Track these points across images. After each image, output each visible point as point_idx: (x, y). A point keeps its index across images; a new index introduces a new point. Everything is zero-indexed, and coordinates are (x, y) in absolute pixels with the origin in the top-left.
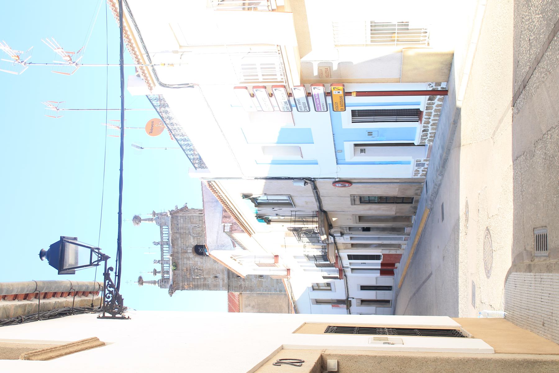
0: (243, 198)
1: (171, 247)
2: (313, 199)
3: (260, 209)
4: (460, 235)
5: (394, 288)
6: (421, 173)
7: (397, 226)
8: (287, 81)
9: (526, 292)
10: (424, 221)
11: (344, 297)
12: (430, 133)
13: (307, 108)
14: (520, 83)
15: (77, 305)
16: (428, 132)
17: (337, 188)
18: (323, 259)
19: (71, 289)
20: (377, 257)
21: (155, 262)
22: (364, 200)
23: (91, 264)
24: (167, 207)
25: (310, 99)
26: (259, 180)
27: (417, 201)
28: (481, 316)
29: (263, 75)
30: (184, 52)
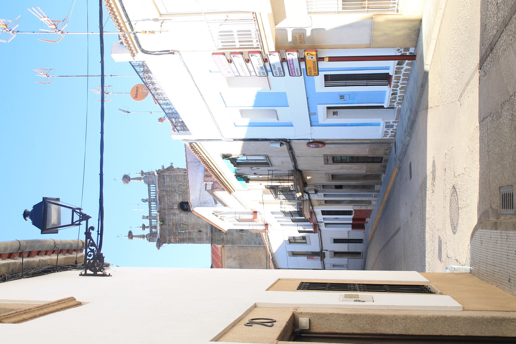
0: (223, 158)
1: (158, 204)
2: (289, 159)
3: (239, 168)
4: (428, 192)
5: (364, 241)
6: (390, 134)
7: (367, 183)
8: (263, 47)
9: (492, 249)
10: (393, 179)
11: (318, 250)
12: (399, 96)
13: (282, 73)
14: (487, 46)
15: (61, 263)
16: (397, 96)
17: (311, 148)
18: (298, 216)
19: (56, 247)
20: (349, 213)
21: (144, 217)
22: (336, 160)
23: (73, 224)
24: (154, 167)
25: (285, 64)
26: (238, 141)
27: (387, 161)
28: (448, 271)
29: (240, 42)
30: (164, 20)
